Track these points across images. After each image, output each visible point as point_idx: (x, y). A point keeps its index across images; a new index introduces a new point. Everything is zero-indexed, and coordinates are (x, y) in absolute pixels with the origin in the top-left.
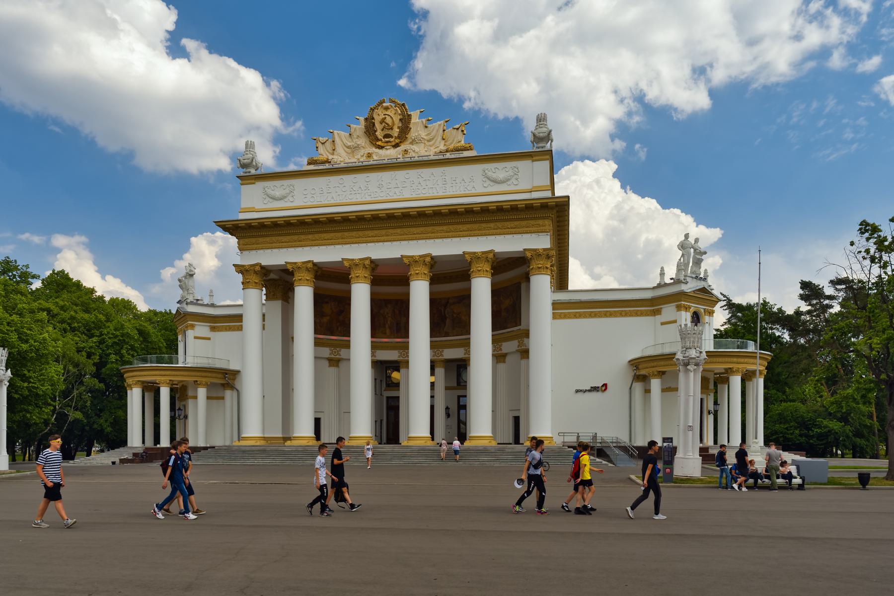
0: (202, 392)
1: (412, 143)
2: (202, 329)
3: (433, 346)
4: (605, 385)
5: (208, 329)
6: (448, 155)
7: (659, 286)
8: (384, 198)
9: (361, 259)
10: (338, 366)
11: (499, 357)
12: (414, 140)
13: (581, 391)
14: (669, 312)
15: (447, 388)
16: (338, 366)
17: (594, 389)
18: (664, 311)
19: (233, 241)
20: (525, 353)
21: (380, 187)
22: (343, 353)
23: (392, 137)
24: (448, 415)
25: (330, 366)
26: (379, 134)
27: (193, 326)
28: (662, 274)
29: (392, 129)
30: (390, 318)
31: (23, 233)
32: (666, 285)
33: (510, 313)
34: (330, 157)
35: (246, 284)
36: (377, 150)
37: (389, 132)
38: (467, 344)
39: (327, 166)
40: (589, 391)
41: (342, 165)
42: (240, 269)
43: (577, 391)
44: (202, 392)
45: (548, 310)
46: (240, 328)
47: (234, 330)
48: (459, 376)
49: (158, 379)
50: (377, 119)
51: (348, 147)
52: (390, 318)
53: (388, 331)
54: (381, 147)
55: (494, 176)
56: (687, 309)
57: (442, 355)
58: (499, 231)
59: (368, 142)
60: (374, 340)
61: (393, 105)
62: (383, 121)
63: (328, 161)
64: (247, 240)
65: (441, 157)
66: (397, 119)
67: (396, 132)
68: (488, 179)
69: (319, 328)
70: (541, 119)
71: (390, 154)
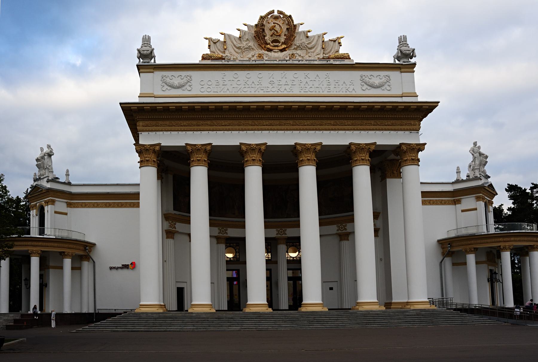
0: (67, 263)
1: (298, 48)
2: (61, 205)
4: (133, 264)
5: (65, 205)
6: (332, 62)
7: (458, 181)
8: (276, 93)
9: (257, 145)
12: (298, 47)
13: (114, 268)
14: (468, 202)
17: (125, 267)
18: (463, 201)
21: (272, 83)
23: (279, 42)
25: (218, 243)
26: (268, 38)
27: (53, 202)
28: (458, 172)
29: (280, 36)
32: (463, 181)
34: (224, 55)
35: (143, 163)
36: (266, 52)
39: (223, 62)
41: (237, 62)
43: (111, 268)
44: (67, 263)
45: (419, 198)
46: (137, 205)
47: (113, 207)
49: (30, 249)
51: (239, 48)
54: (270, 50)
55: (371, 81)
56: (483, 199)
57: (345, 229)
58: (256, 127)
59: (256, 45)
60: (212, 218)
61: (282, 16)
62: (272, 29)
63: (222, 58)
64: (147, 122)
65: (325, 62)
66: (284, 27)
67: (282, 39)
68: (366, 83)
71: (276, 56)
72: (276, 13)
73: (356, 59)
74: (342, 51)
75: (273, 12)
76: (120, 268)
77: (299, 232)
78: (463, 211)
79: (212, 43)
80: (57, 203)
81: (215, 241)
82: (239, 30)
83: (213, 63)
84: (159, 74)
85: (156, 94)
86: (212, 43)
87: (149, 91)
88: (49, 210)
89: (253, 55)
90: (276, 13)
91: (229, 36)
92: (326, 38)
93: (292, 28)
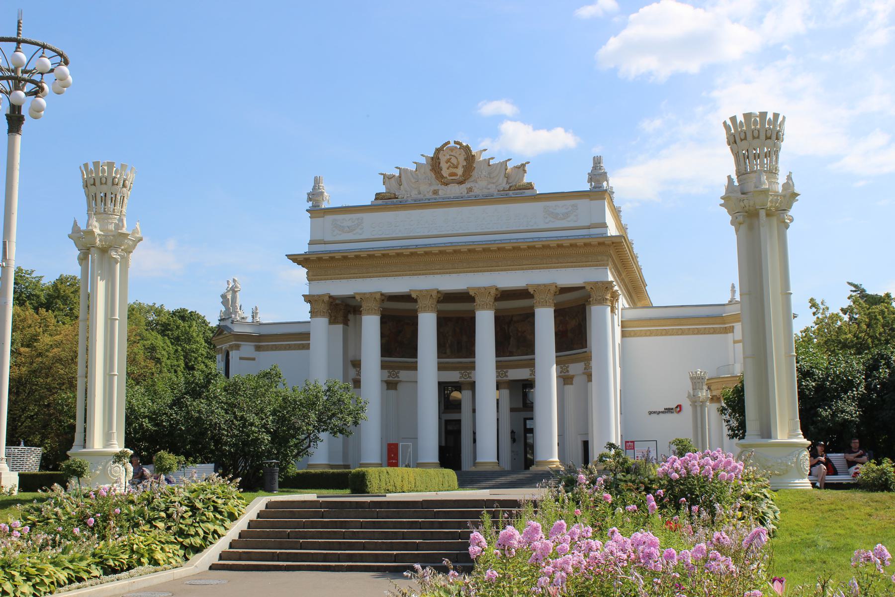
3: (499, 366)
4: (679, 406)
5: (253, 349)
10: (396, 389)
11: (565, 379)
15: (512, 410)
16: (396, 389)
17: (669, 410)
19: (302, 272)
20: (589, 377)
22: (403, 375)
24: (514, 440)
26: (445, 173)
27: (237, 347)
30: (457, 338)
31: (605, 42)
33: (574, 335)
37: (454, 170)
38: (531, 364)
40: (663, 412)
42: (308, 299)
43: (650, 413)
46: (307, 347)
48: (525, 396)
50: (443, 159)
52: (457, 338)
53: (448, 351)
57: (506, 376)
62: (448, 161)
67: (460, 171)
69: (387, 350)
70: (776, 116)
72: (452, 144)
73: (539, 189)
74: (526, 179)
75: (448, 143)
76: (663, 412)
77: (439, 376)
78: (241, 358)
79: (387, 178)
80: (242, 348)
81: (385, 385)
82: (382, 174)
83: (386, 201)
84: (329, 218)
85: (328, 238)
86: (387, 178)
87: (319, 237)
88: (233, 355)
89: (426, 189)
90: (452, 144)
91: (406, 170)
92: (510, 165)
93: (470, 158)
